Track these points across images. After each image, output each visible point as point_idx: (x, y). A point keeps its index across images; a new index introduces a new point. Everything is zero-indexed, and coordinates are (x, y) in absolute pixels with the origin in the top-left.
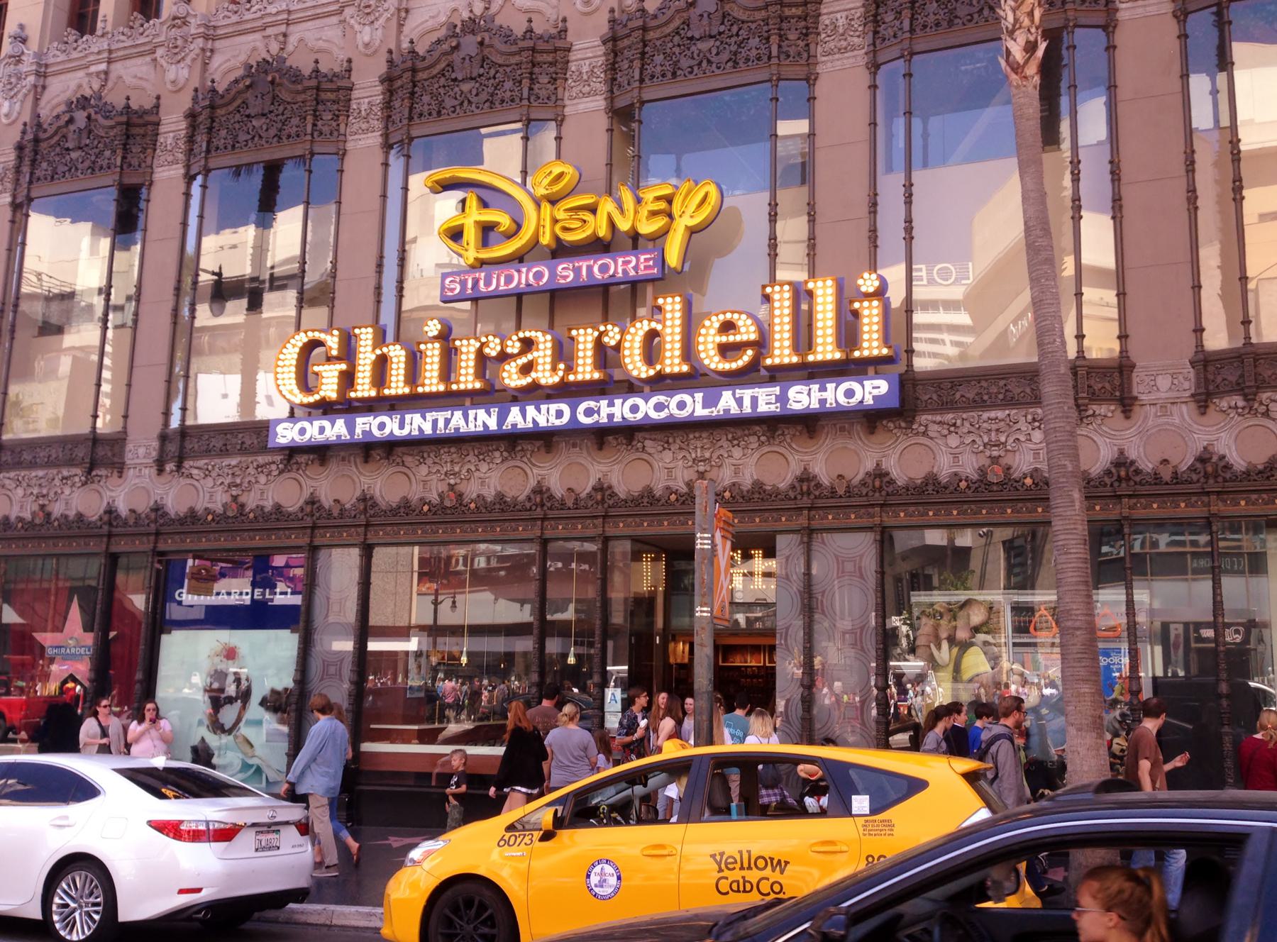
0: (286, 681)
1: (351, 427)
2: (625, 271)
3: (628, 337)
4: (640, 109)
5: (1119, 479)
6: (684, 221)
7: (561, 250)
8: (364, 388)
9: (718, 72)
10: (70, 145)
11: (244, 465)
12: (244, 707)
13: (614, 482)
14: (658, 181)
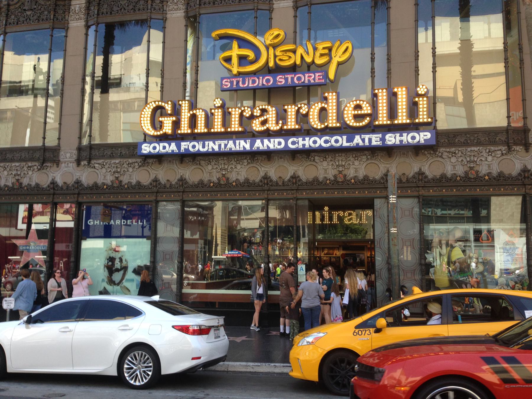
0: (145, 261)
1: (383, 139)
2: (309, 80)
3: (312, 110)
4: (199, 17)
5: (525, 177)
6: (336, 60)
7: (278, 70)
8: (185, 129)
9: (33, 23)
10: (26, 8)
11: (122, 163)
12: (124, 274)
13: (187, 177)
14: (320, 42)
